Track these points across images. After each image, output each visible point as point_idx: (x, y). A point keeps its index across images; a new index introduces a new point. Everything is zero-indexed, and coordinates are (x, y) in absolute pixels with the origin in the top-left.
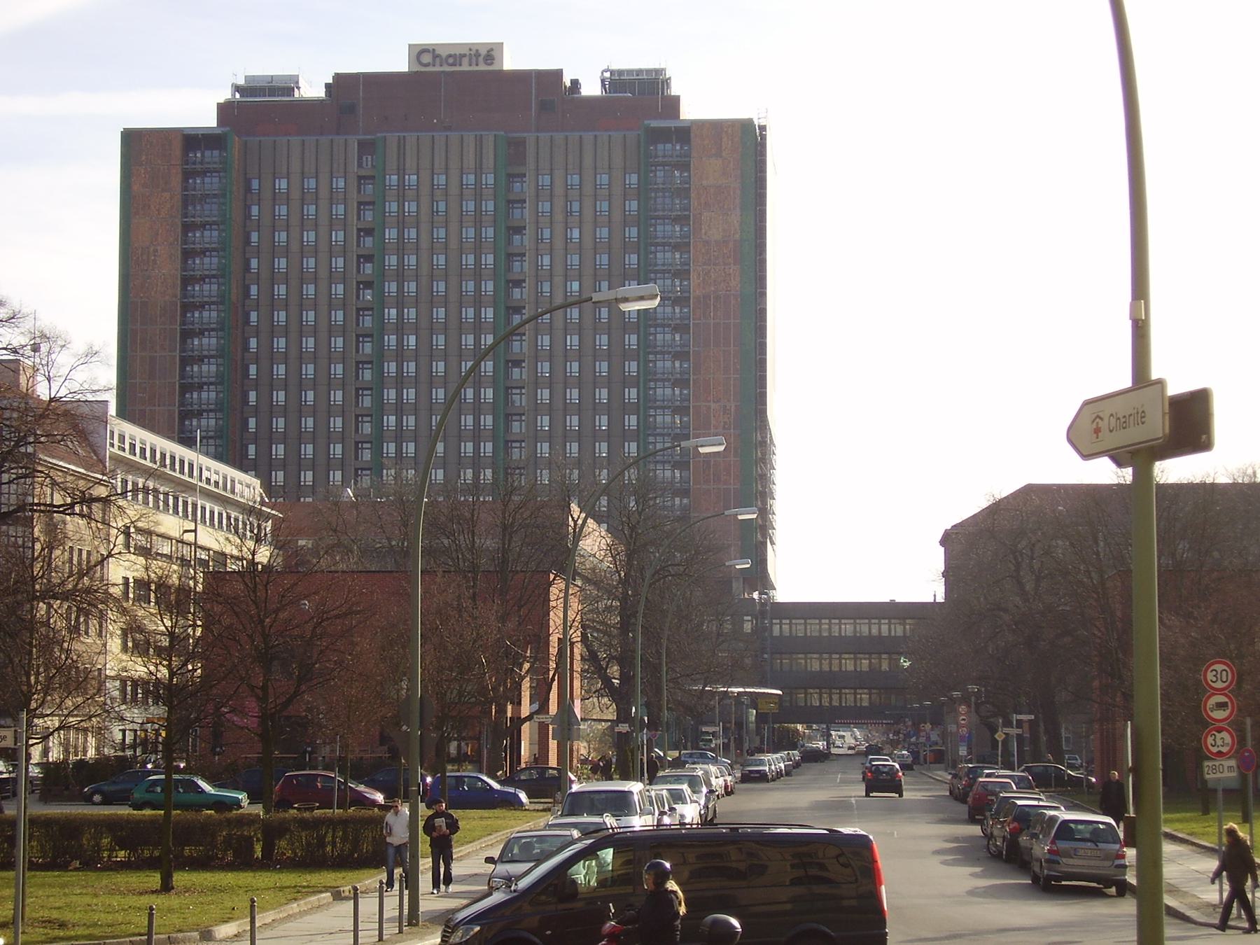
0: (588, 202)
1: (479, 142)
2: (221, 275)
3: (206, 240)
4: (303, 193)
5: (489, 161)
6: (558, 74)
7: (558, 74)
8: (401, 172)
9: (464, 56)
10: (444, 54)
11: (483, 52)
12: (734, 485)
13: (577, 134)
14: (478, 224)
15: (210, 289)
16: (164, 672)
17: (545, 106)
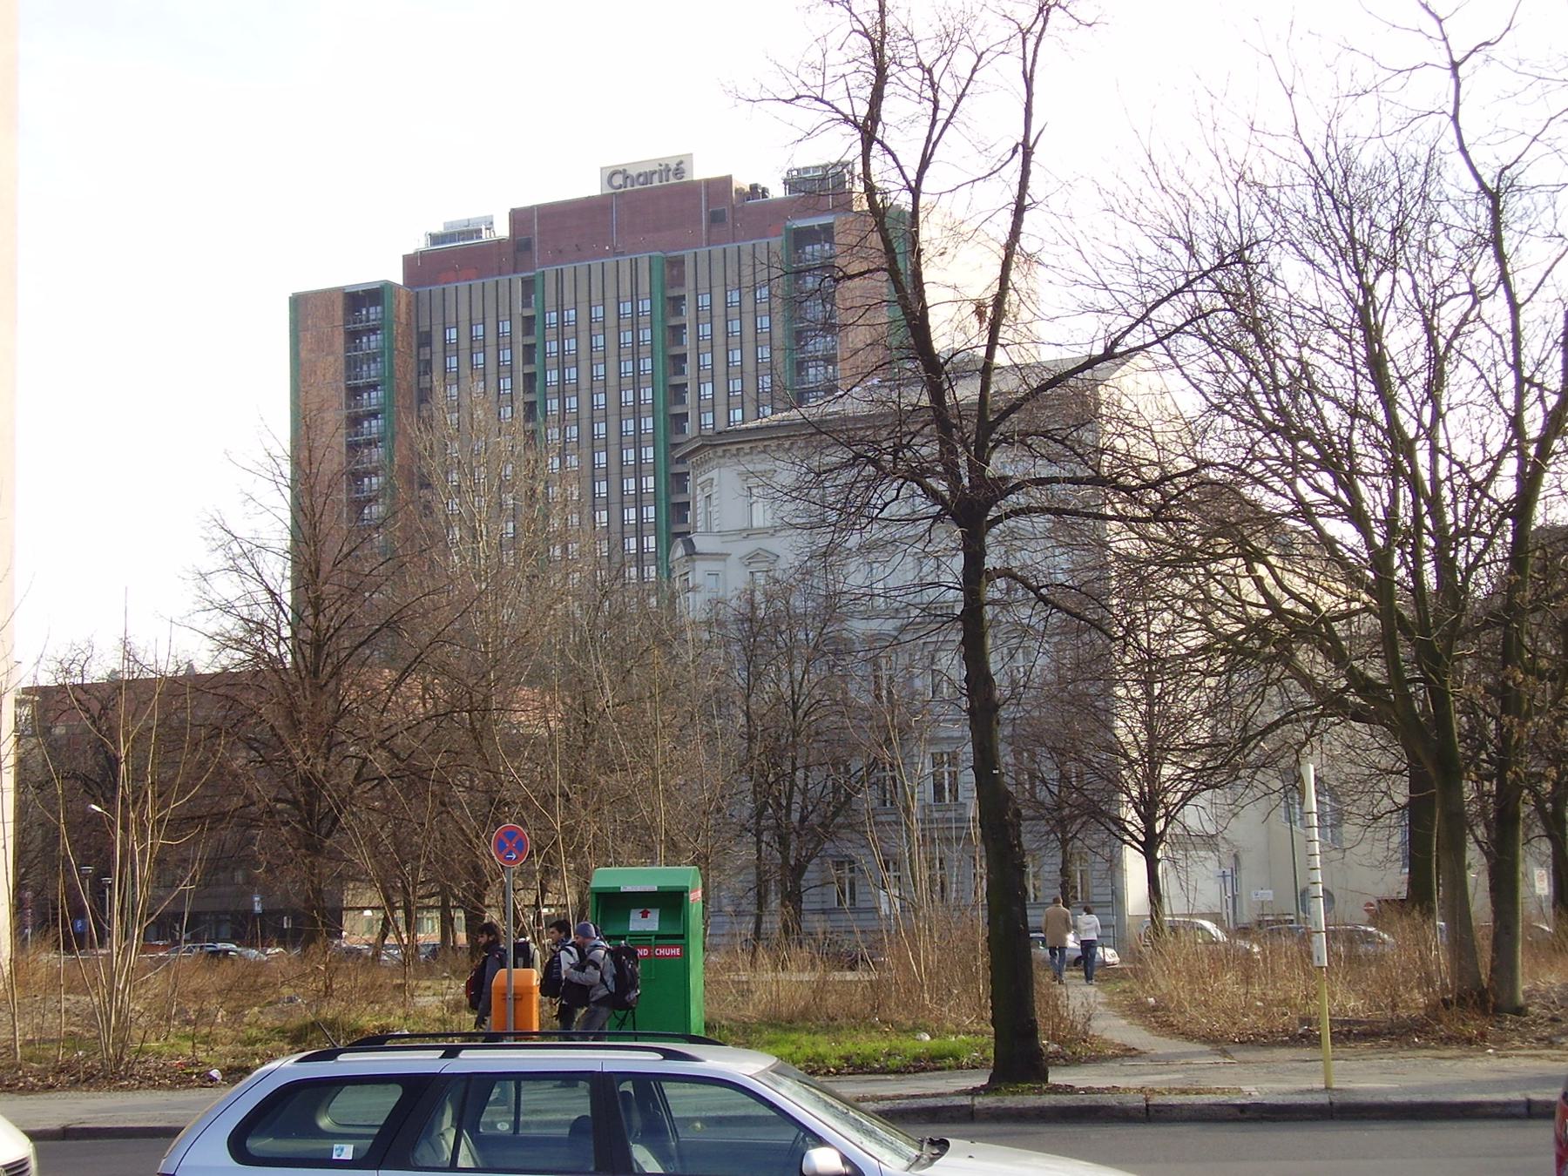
0: (748, 319)
1: (634, 266)
4: (472, 340)
5: (644, 287)
6: (727, 181)
7: (727, 181)
8: (560, 309)
9: (654, 173)
10: (633, 172)
11: (673, 166)
13: (721, 247)
16: (1553, 652)
17: (716, 218)
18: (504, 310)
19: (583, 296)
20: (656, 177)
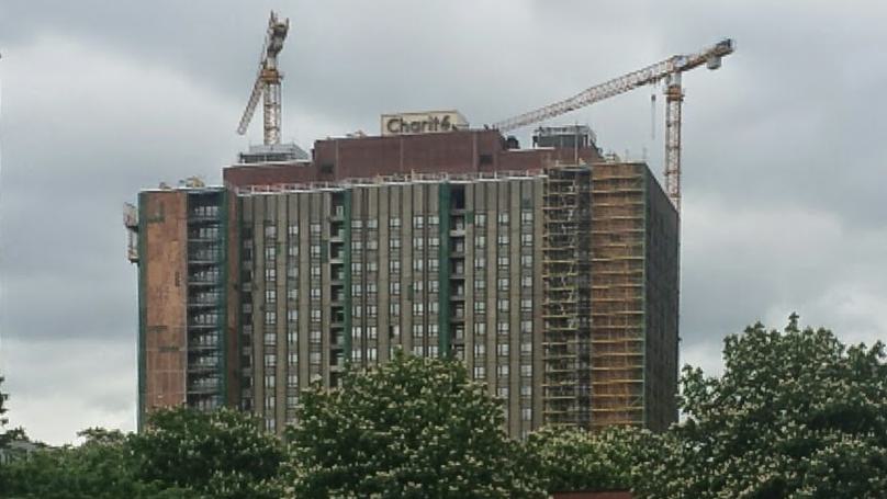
2: (222, 306)
3: (209, 214)
5: (435, 206)
8: (365, 218)
10: (409, 120)
12: (573, 344)
14: (426, 323)
15: (212, 319)
16: (855, 373)
18: (316, 215)
19: (384, 208)
20: (427, 127)
